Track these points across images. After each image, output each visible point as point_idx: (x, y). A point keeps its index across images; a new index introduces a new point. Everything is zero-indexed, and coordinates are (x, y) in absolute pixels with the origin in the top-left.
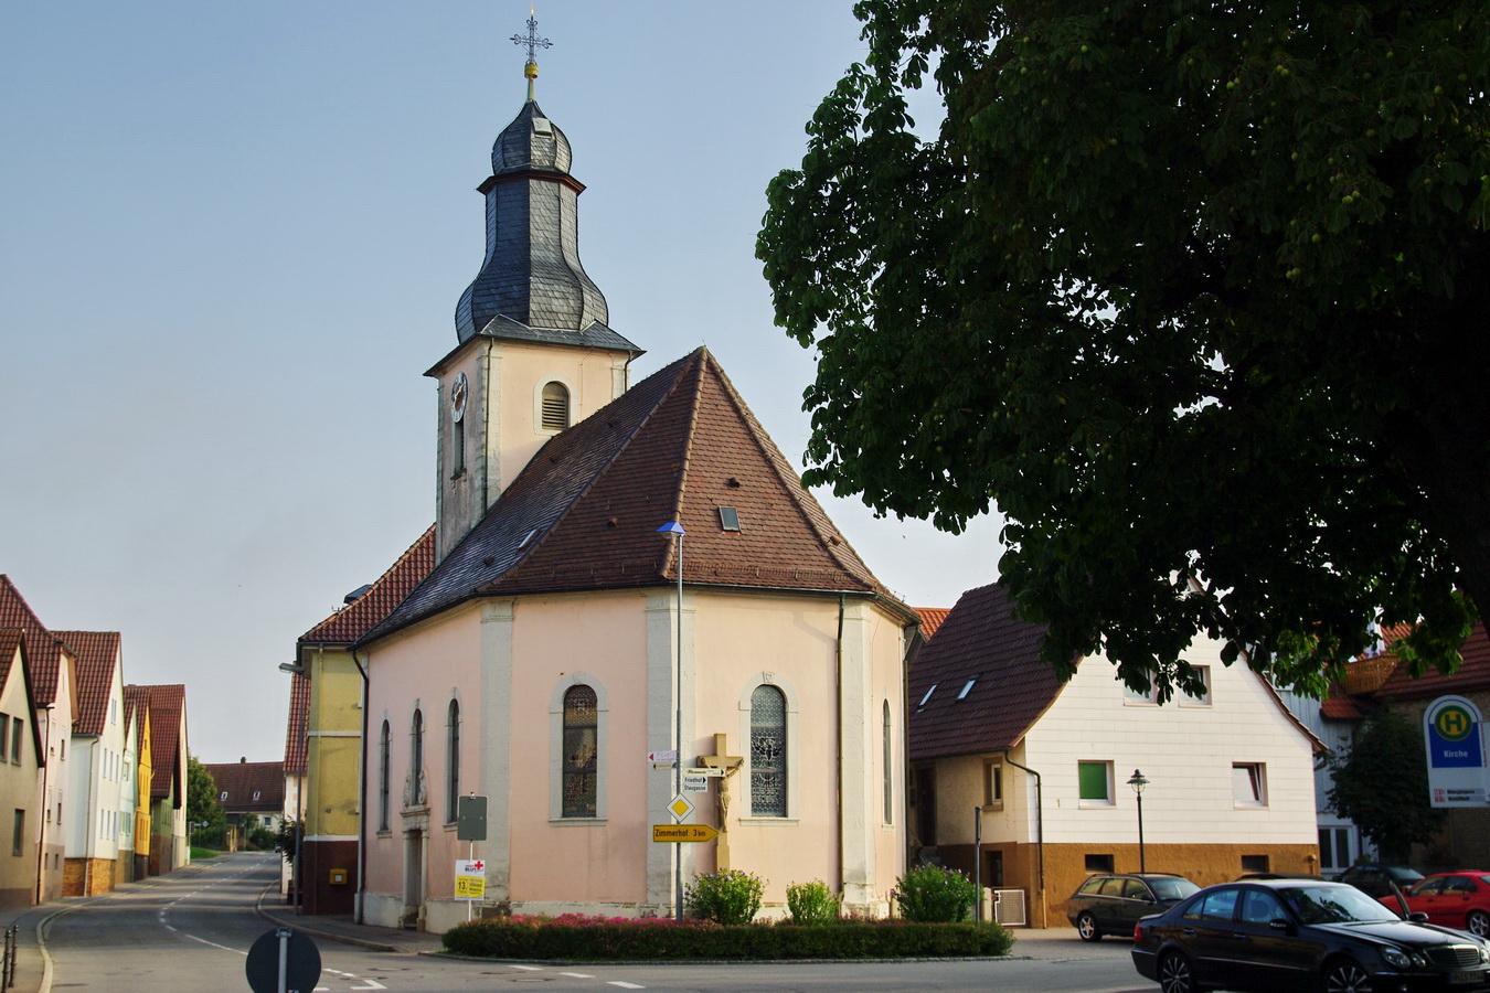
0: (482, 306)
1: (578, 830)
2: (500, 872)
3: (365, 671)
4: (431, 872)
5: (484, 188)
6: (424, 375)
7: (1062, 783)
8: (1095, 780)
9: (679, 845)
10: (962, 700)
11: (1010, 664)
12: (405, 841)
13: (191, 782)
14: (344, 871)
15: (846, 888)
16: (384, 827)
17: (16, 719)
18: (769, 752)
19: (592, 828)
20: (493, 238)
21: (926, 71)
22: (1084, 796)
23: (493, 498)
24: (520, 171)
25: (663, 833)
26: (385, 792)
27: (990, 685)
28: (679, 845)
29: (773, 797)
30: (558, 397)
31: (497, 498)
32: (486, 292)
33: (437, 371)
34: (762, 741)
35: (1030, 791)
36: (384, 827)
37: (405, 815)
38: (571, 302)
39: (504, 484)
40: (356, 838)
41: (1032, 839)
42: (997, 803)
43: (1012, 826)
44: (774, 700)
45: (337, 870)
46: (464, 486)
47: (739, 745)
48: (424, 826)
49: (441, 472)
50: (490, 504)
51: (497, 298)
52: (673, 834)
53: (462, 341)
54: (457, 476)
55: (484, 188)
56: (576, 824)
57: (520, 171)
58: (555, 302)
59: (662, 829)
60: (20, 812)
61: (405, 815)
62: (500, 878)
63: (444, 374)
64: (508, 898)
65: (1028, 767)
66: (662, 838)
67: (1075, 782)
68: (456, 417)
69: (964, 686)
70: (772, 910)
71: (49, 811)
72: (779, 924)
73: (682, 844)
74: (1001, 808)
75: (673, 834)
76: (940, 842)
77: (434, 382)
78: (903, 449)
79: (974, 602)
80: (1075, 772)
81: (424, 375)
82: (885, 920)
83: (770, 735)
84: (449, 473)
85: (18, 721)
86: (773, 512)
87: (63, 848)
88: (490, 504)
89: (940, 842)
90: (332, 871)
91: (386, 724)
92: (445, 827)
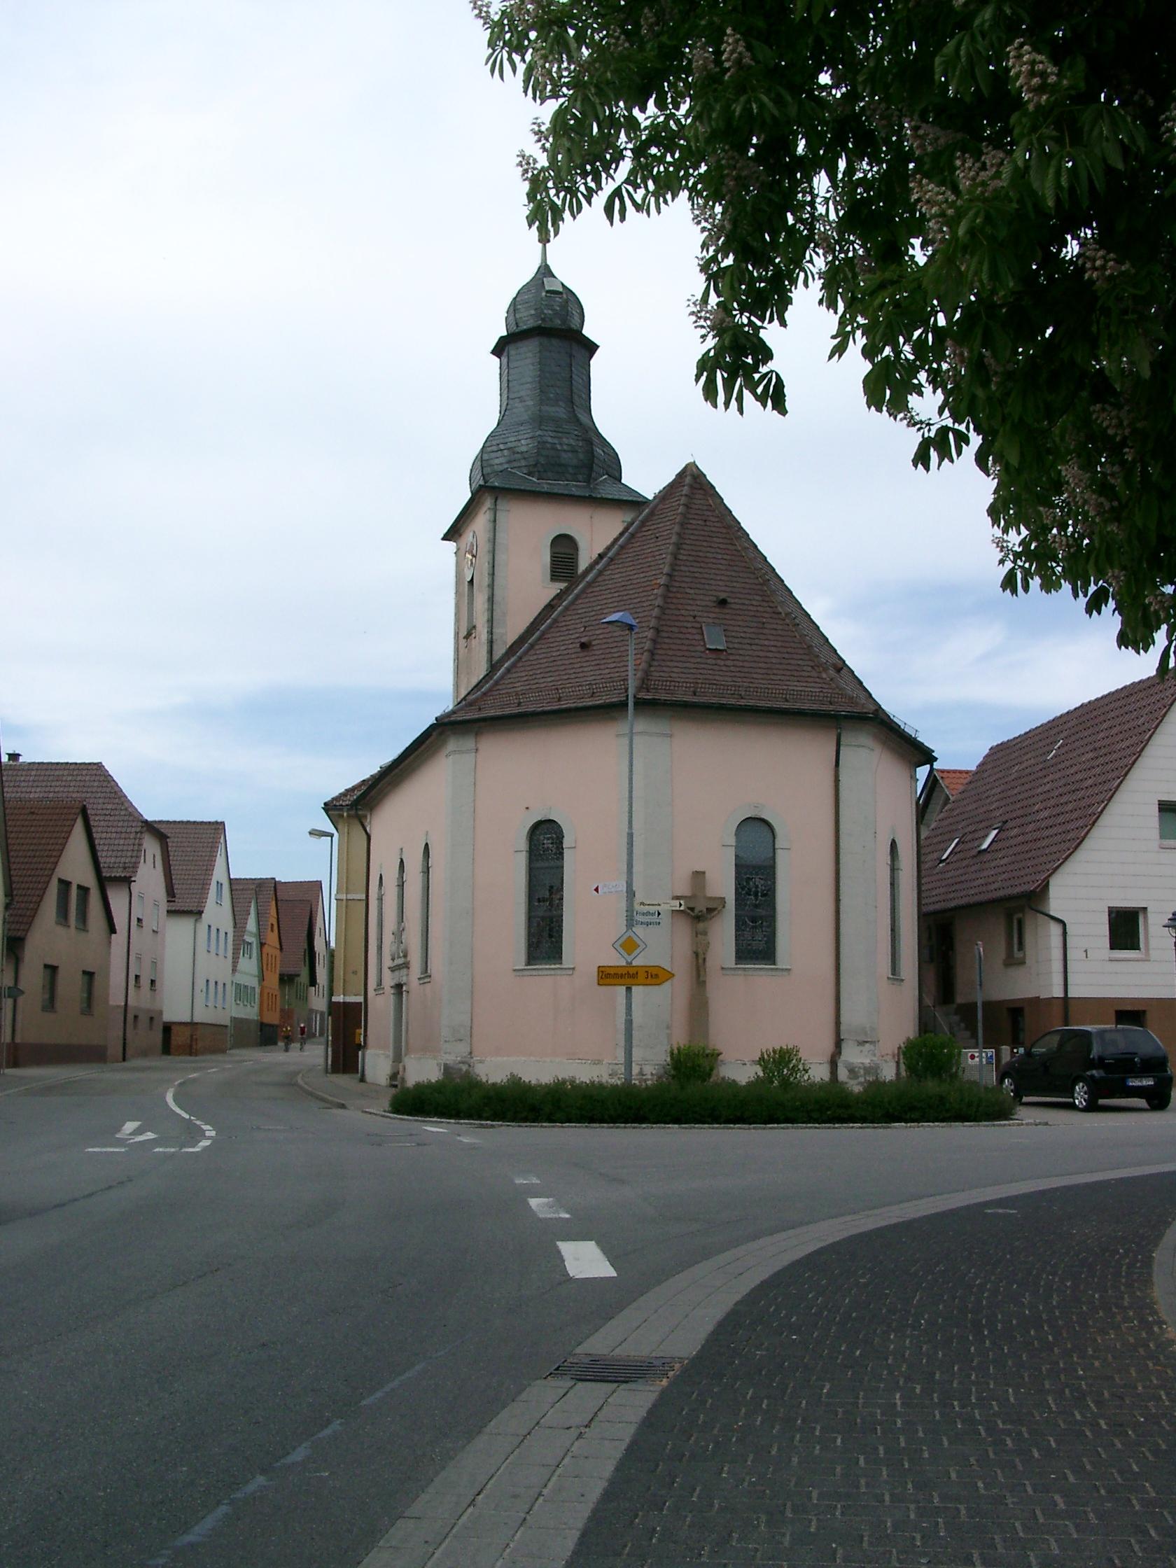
0: (492, 462)
1: (544, 981)
6: (444, 539)
7: (1091, 931)
8: (1125, 928)
9: (629, 989)
10: (985, 850)
11: (1036, 808)
15: (844, 1045)
16: (380, 983)
17: (79, 887)
18: (756, 895)
20: (505, 397)
21: (967, 444)
22: (1113, 946)
23: (499, 652)
25: (608, 976)
26: (380, 948)
27: (1015, 831)
28: (629, 989)
29: (757, 944)
31: (503, 651)
32: (495, 448)
34: (749, 879)
35: (1056, 941)
36: (380, 983)
37: (392, 969)
40: (360, 999)
41: (1058, 992)
42: (1018, 955)
43: (1041, 978)
44: (756, 829)
46: (474, 642)
47: (723, 885)
48: (404, 980)
49: (457, 634)
51: (506, 452)
52: (622, 976)
54: (468, 636)
55: (498, 351)
58: (564, 455)
59: (608, 971)
60: (89, 975)
61: (392, 969)
63: (460, 535)
65: (1052, 913)
66: (608, 981)
67: (1105, 930)
69: (987, 836)
70: (739, 1069)
71: (137, 977)
72: (750, 1084)
73: (634, 988)
74: (1022, 962)
75: (622, 976)
76: (960, 1000)
77: (451, 546)
78: (809, 166)
79: (999, 755)
80: (1105, 918)
81: (444, 539)
82: (822, 1086)
83: (757, 874)
84: (464, 633)
85: (84, 890)
86: (765, 631)
87: (161, 1013)
89: (960, 1000)
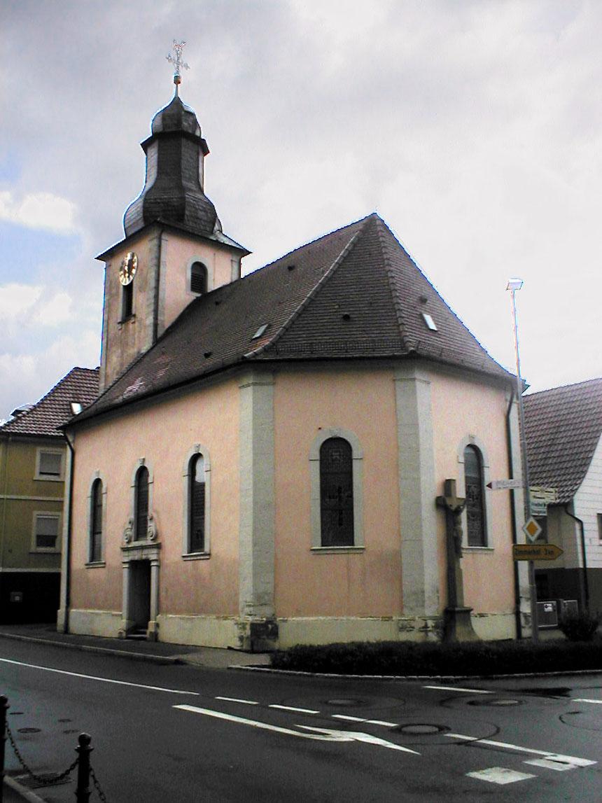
1: (338, 560)
2: (266, 593)
3: (72, 445)
4: (163, 594)
5: (146, 145)
6: (98, 258)
12: (126, 570)
13: (40, 494)
14: (20, 593)
19: (351, 556)
24: (176, 139)
30: (199, 275)
33: (107, 256)
36: (95, 554)
38: (209, 215)
39: (167, 324)
45: (17, 593)
50: (159, 336)
51: (162, 205)
53: (129, 235)
56: (337, 552)
57: (176, 139)
62: (266, 597)
64: (274, 615)
68: (125, 281)
77: (103, 264)
88: (159, 336)
90: (13, 593)
91: (97, 483)
92: (86, 565)
